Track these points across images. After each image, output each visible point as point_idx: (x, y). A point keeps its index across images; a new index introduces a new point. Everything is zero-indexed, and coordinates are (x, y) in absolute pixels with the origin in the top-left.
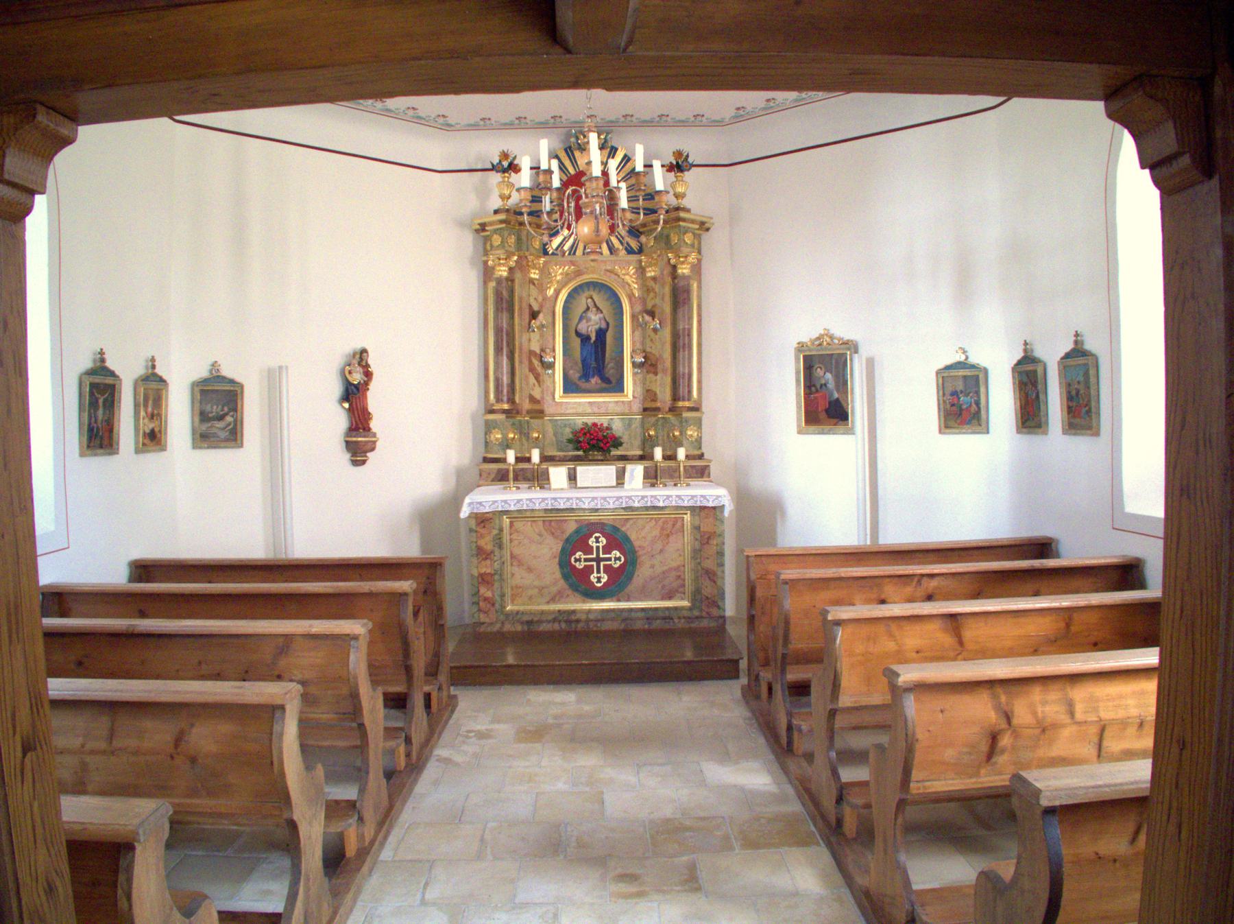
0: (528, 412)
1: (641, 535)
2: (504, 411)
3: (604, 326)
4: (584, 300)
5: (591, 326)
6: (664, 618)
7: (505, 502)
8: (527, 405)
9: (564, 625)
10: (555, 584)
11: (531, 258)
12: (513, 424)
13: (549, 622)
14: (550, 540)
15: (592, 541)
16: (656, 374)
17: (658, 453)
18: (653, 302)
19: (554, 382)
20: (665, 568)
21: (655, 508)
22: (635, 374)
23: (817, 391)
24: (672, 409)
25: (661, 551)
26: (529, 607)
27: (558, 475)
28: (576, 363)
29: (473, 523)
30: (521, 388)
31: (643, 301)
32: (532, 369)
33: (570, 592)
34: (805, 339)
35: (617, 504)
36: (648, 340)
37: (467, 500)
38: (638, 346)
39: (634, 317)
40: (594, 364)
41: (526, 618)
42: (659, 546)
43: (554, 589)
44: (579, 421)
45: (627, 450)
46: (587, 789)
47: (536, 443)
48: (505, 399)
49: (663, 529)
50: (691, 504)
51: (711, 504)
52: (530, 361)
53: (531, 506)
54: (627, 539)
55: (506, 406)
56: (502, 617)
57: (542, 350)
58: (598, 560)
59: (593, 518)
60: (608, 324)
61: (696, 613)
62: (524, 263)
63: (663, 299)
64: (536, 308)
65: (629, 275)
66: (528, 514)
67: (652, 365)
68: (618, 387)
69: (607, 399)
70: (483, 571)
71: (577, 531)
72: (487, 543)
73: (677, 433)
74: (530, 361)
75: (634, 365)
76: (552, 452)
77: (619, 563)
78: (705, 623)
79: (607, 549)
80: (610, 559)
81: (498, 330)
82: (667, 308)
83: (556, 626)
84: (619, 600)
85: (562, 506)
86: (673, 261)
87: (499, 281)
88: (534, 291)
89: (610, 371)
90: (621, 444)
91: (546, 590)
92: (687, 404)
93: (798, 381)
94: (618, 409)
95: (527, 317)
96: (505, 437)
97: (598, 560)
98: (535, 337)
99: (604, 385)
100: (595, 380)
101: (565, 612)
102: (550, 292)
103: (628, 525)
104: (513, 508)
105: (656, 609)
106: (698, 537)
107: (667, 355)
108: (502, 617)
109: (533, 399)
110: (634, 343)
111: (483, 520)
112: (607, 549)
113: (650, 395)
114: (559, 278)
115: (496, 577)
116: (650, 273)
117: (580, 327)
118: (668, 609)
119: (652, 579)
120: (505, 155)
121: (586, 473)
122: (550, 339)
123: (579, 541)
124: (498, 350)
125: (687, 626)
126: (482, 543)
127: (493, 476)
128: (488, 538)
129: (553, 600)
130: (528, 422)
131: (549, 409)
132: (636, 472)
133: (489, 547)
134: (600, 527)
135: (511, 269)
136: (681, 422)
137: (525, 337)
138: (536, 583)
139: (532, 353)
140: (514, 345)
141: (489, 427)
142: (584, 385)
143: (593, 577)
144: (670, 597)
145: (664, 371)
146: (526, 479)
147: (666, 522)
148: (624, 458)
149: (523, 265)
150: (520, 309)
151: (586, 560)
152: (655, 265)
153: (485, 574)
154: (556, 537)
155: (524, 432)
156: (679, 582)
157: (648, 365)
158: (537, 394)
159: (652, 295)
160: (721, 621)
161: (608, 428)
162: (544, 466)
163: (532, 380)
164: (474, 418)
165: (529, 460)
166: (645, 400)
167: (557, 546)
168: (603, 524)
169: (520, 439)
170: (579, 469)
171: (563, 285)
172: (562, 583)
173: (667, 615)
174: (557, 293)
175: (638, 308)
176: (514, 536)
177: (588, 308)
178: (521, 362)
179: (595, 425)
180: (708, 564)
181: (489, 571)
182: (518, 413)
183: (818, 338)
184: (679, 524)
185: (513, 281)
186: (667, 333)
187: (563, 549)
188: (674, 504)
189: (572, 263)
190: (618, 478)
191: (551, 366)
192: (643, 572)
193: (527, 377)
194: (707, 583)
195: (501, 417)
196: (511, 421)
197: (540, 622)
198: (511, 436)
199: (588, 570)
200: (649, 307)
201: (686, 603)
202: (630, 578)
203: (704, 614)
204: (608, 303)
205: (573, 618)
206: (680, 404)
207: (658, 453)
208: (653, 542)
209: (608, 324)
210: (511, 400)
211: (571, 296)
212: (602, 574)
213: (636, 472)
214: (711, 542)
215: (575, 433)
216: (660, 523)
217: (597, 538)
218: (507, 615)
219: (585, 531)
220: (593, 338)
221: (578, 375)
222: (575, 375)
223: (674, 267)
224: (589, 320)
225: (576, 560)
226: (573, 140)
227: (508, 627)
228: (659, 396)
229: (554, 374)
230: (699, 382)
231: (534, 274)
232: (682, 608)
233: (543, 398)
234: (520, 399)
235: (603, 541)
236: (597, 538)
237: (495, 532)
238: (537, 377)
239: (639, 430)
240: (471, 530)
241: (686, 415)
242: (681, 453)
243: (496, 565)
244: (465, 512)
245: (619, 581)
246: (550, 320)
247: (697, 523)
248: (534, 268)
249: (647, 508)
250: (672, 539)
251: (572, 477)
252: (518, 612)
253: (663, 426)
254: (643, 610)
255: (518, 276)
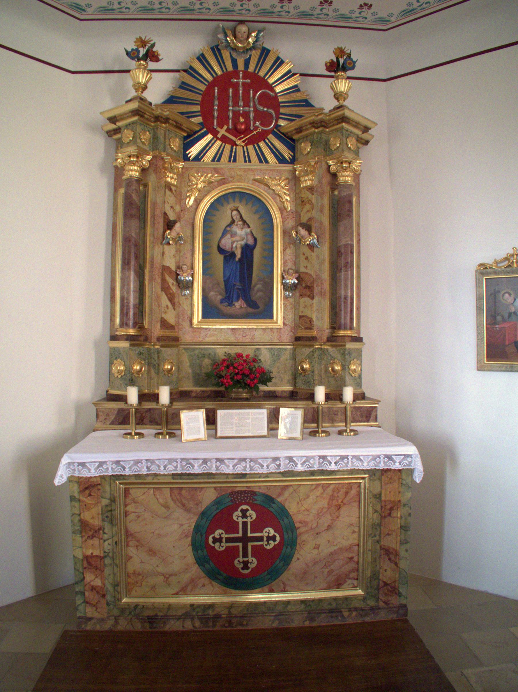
0: (159, 339)
1: (302, 508)
2: (129, 338)
3: (251, 242)
4: (229, 212)
5: (237, 239)
6: (331, 611)
7: (117, 463)
8: (157, 331)
9: (197, 624)
10: (187, 570)
11: (167, 159)
12: (140, 353)
13: (179, 618)
14: (178, 513)
15: (237, 516)
16: (312, 298)
17: (320, 393)
18: (309, 215)
19: (192, 305)
20: (333, 548)
21: (323, 472)
22: (285, 298)
23: (504, 321)
24: (332, 339)
25: (329, 527)
26: (153, 600)
27: (192, 421)
28: (218, 284)
29: (75, 489)
30: (151, 310)
31: (297, 214)
32: (165, 288)
33: (206, 581)
34: (489, 260)
35: (273, 468)
36: (302, 258)
37: (65, 460)
38: (290, 265)
39: (285, 233)
40: (238, 285)
41: (147, 613)
42: (326, 520)
43: (185, 578)
44: (221, 352)
45: (276, 385)
46: (222, 572)
47: (167, 378)
48: (131, 323)
49: (332, 498)
50: (372, 466)
51: (397, 466)
52: (164, 280)
53: (154, 470)
54: (284, 512)
55: (132, 332)
56: (116, 612)
57: (179, 267)
58: (245, 540)
59: (241, 486)
60: (255, 240)
61: (372, 603)
62: (160, 163)
63: (321, 211)
64: (172, 217)
65: (281, 187)
66: (149, 480)
67: (307, 287)
68: (267, 313)
69: (254, 326)
70: (89, 552)
71: (217, 502)
72: (93, 516)
73: (337, 368)
74: (164, 280)
75: (285, 287)
76: (188, 386)
77: (272, 544)
78: (383, 616)
79: (258, 526)
80: (261, 539)
81: (126, 240)
82: (326, 220)
83: (188, 625)
84: (271, 591)
85: (196, 471)
86: (333, 169)
87: (130, 182)
88: (171, 199)
89: (257, 294)
90: (269, 380)
91: (173, 579)
92: (349, 333)
93: (479, 309)
94: (266, 338)
95: (161, 226)
96: (129, 369)
97: (245, 540)
98: (170, 250)
99: (250, 310)
100: (239, 304)
101: (199, 606)
102: (191, 202)
103: (286, 494)
104: (127, 472)
105: (320, 600)
106: (378, 508)
107: (326, 276)
108: (116, 612)
109: (164, 324)
110: (284, 263)
111: (88, 486)
112: (258, 526)
113: (304, 321)
114: (200, 186)
115: (107, 561)
116: (307, 182)
117: (223, 242)
118: (335, 599)
119: (315, 563)
120: (143, 43)
121: (229, 419)
122: (189, 255)
123: (220, 515)
124: (126, 263)
125: (360, 621)
126: (87, 516)
127: (112, 418)
128: (96, 510)
129: (183, 591)
130: (158, 352)
131: (187, 337)
132: (291, 417)
133: (96, 522)
134: (247, 496)
135: (144, 171)
136: (343, 354)
137: (158, 250)
138: (161, 569)
139: (165, 269)
140: (144, 259)
141: (114, 355)
142: (225, 309)
143: (238, 563)
144: (338, 585)
145: (322, 294)
146: (154, 422)
147: (337, 489)
148: (272, 396)
149: (156, 167)
150: (154, 216)
151: (228, 540)
152: (312, 172)
153: (92, 556)
154: (187, 510)
155: (152, 363)
156: (353, 565)
157: (302, 287)
158: (171, 317)
159: (308, 207)
160: (402, 611)
161: (255, 360)
162: (177, 405)
163: (165, 300)
164: (97, 344)
165: (155, 397)
166: (295, 328)
167: (189, 522)
168: (254, 493)
169: (149, 372)
170: (220, 413)
171: (204, 193)
172: (195, 570)
173: (335, 607)
174: (198, 202)
175: (291, 223)
176: (130, 508)
177: (233, 222)
178: (152, 280)
179: (239, 355)
180: (390, 542)
181: (96, 553)
182: (146, 339)
183: (506, 259)
184: (353, 492)
185: (146, 185)
186: (325, 251)
187: (197, 528)
188: (350, 467)
189: (216, 171)
190: (270, 422)
191: (189, 285)
192: (305, 554)
193: (158, 298)
194: (387, 565)
195: (125, 344)
196: (138, 349)
197: (166, 618)
198: (137, 367)
199: (232, 553)
200: (304, 220)
201: (359, 592)
202: (287, 560)
203: (381, 604)
204: (256, 216)
205: (211, 612)
206: (342, 333)
207: (320, 393)
208: (320, 515)
209: (255, 240)
210: (139, 325)
211: (213, 207)
212: (250, 559)
213: (291, 417)
214: (394, 514)
215: (216, 364)
216: (329, 491)
217: (244, 512)
218: (123, 610)
219: (227, 501)
220: (238, 256)
221: (219, 297)
222: (216, 297)
223: (334, 176)
224: (233, 235)
225: (215, 540)
226: (221, 36)
227: (123, 625)
228: (316, 322)
229: (192, 295)
230: (358, 309)
231: (171, 178)
232: (355, 597)
233: (178, 323)
234: (150, 323)
235: (252, 514)
236: (244, 512)
237: (105, 502)
238: (171, 298)
239: (290, 363)
240: (72, 498)
241: (350, 346)
242: (348, 394)
243: (107, 546)
244: (61, 478)
245: (271, 568)
246: (189, 232)
247: (377, 490)
248: (171, 170)
249: (312, 473)
250: (344, 511)
251: (211, 420)
252: (136, 606)
253: (320, 358)
254: (303, 602)
255: (152, 179)
